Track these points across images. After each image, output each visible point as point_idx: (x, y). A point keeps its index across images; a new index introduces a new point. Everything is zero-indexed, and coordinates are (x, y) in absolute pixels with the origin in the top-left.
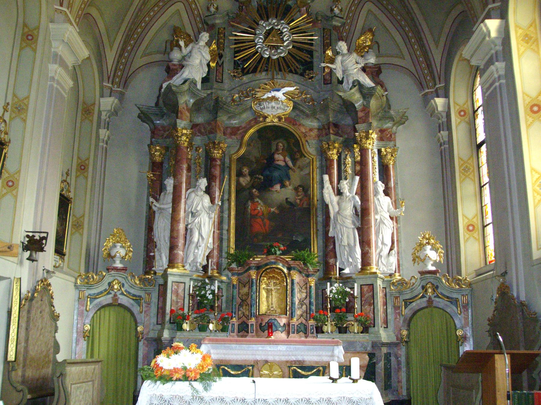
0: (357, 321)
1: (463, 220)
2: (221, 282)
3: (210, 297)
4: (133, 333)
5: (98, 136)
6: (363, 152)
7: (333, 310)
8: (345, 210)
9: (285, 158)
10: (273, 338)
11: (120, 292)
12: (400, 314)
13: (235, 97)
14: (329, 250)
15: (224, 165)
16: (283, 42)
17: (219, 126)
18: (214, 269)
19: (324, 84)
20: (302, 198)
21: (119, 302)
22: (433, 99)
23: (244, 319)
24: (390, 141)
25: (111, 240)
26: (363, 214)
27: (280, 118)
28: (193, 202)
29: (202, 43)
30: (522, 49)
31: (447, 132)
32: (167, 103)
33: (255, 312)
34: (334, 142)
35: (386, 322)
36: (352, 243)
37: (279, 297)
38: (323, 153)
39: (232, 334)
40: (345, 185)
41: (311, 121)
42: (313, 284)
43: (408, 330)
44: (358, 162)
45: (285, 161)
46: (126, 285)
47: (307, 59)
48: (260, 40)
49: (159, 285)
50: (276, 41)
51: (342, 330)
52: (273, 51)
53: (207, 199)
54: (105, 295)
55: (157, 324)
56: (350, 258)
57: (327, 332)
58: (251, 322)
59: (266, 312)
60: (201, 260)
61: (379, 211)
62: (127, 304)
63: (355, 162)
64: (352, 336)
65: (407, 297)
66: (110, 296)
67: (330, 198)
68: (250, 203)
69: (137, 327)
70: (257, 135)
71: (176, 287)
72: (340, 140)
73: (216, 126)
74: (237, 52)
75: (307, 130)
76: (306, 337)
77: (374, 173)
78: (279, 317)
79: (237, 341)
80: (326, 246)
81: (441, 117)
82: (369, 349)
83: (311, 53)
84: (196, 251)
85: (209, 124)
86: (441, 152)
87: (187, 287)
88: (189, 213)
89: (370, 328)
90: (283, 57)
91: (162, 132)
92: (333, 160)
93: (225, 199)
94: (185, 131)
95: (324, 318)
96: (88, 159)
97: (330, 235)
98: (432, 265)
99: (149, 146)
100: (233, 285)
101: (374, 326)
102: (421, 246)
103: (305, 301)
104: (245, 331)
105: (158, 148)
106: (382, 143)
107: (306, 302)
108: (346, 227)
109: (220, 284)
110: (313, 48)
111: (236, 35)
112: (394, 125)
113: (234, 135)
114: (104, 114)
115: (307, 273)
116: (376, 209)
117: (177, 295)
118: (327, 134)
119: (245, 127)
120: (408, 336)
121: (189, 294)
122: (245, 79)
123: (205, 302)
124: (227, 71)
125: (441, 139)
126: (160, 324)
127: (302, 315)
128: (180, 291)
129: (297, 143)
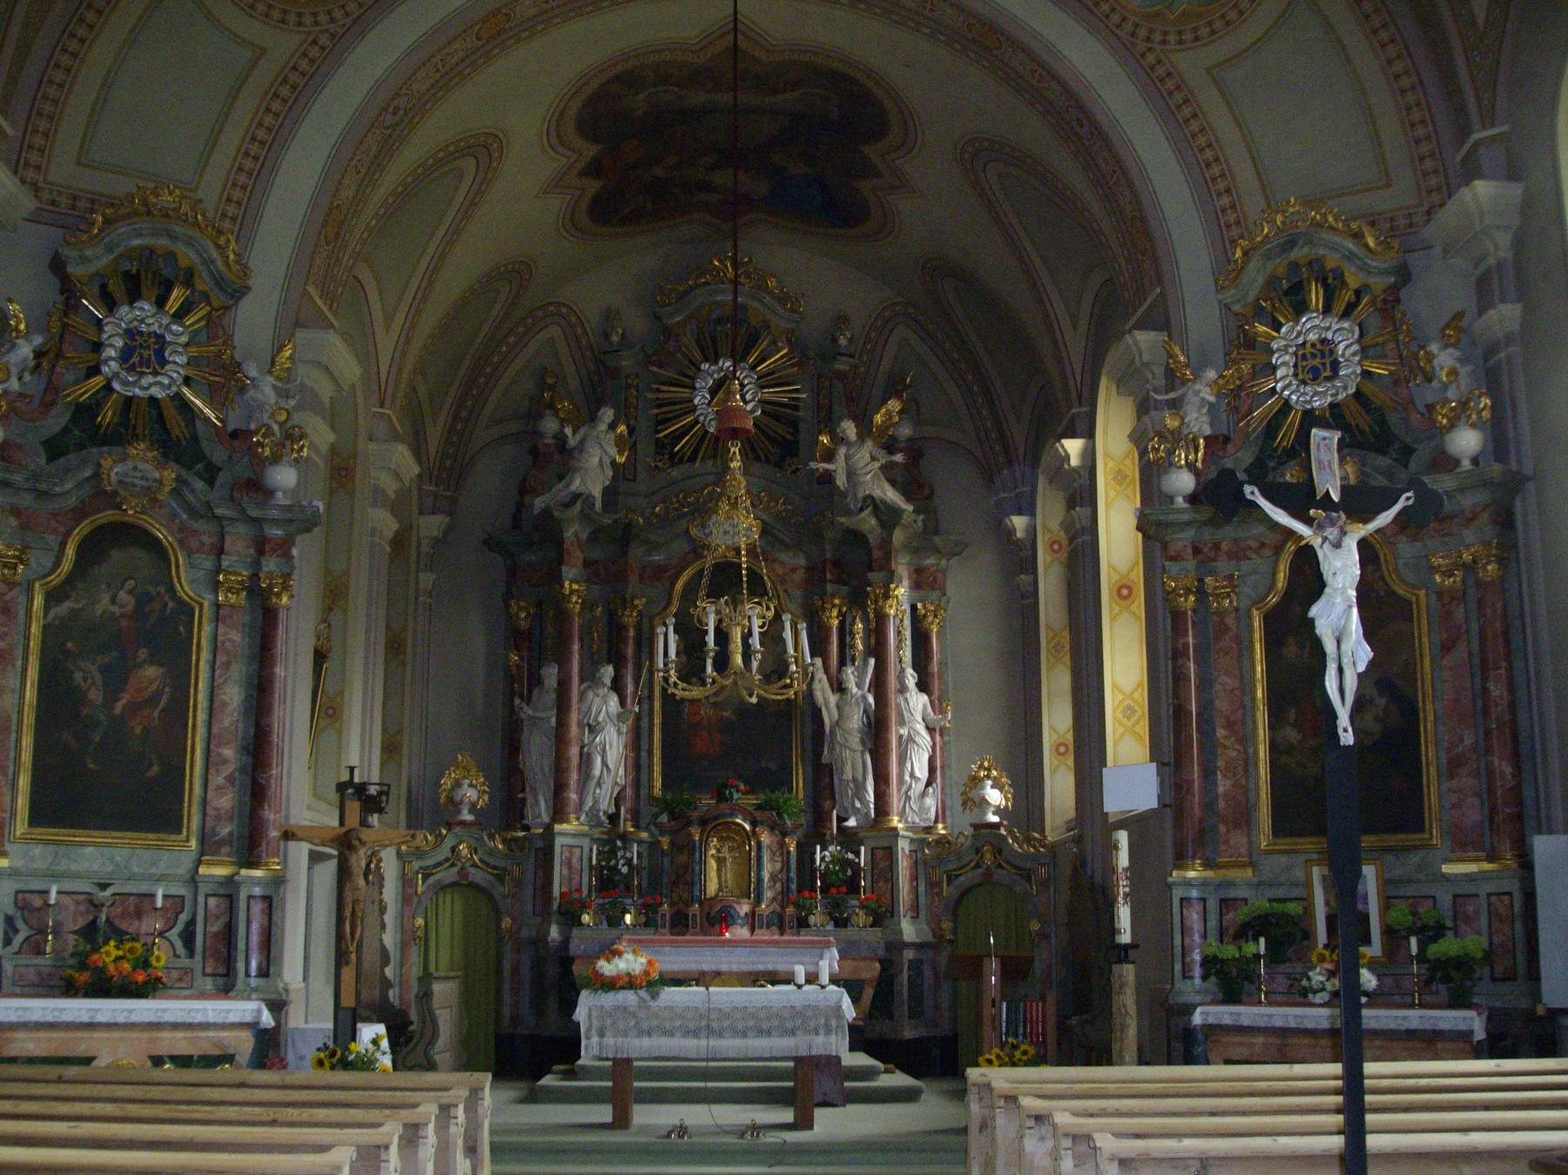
0: (862, 907)
2: (640, 842)
3: (625, 870)
6: (881, 618)
12: (939, 894)
22: (1008, 515)
23: (681, 906)
24: (933, 589)
26: (877, 729)
28: (590, 708)
29: (603, 427)
30: (1112, 493)
34: (833, 596)
36: (860, 777)
40: (850, 674)
43: (955, 921)
60: (606, 805)
62: (482, 883)
65: (951, 866)
66: (455, 869)
69: (499, 920)
74: (661, 422)
77: (901, 652)
82: (881, 952)
83: (794, 424)
87: (586, 851)
94: (575, 587)
98: (994, 813)
102: (976, 782)
107: (780, 877)
114: (424, 542)
116: (900, 715)
117: (570, 866)
121: (591, 867)
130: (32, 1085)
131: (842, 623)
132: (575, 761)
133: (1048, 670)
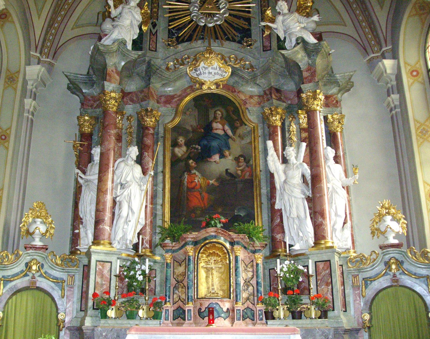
1: (424, 187)
3: (140, 278)
4: (54, 322)
5: (22, 104)
6: (311, 115)
7: (285, 291)
8: (293, 178)
9: (223, 127)
10: (214, 326)
11: (39, 274)
13: (169, 65)
14: (275, 224)
15: (158, 134)
16: (219, 9)
17: (152, 94)
18: (146, 248)
19: (263, 51)
20: (244, 168)
21: (38, 285)
23: (180, 303)
25: (30, 215)
26: (315, 181)
27: (217, 85)
28: (122, 172)
31: (398, 95)
32: (98, 71)
33: (193, 295)
34: (277, 107)
35: (345, 305)
36: (302, 215)
37: (220, 277)
38: (265, 119)
39: (165, 322)
40: (291, 151)
41: (251, 88)
42: (260, 261)
43: (370, 314)
44: (304, 130)
45: (224, 130)
46: (45, 266)
47: (244, 26)
48: (196, 9)
49: (84, 266)
50: (212, 9)
51: (296, 315)
52: (209, 19)
53: (138, 169)
54: (22, 277)
55: (81, 310)
56: (300, 232)
57: (279, 318)
58: (189, 307)
59: (206, 296)
60: (132, 237)
61: (330, 179)
63: (301, 129)
64: (308, 322)
65: (367, 275)
67: (275, 166)
68: (186, 175)
70: (193, 103)
71: (100, 267)
72: (283, 105)
73: (148, 93)
75: (247, 98)
76: (254, 324)
78: (221, 301)
79: (169, 331)
80: (272, 220)
81: (389, 81)
83: (248, 20)
84: (126, 227)
85: (142, 91)
86: (392, 117)
88: (117, 185)
89: (329, 312)
90: (220, 25)
91: (92, 102)
92: (276, 126)
93: (158, 171)
94: (113, 95)
95: (275, 302)
96: (10, 128)
97: (277, 207)
98: (394, 238)
99: (78, 118)
100: (167, 264)
101: (333, 310)
102: (381, 217)
103: (251, 282)
104: (181, 318)
105: (87, 118)
106: (327, 109)
108: (295, 197)
109: (152, 264)
110: (251, 15)
111: (170, 4)
112: (339, 91)
113: (169, 103)
114: (30, 83)
115: (253, 249)
117: (102, 276)
118: (268, 100)
119: (180, 95)
120: (370, 320)
122: (180, 47)
123: (135, 284)
124: (161, 40)
125: (391, 103)
126: (83, 311)
127: (248, 299)
128: (106, 272)
129: (236, 111)
130: (274, 326)
131: (283, 124)
132: (109, 204)
133: (419, 146)
